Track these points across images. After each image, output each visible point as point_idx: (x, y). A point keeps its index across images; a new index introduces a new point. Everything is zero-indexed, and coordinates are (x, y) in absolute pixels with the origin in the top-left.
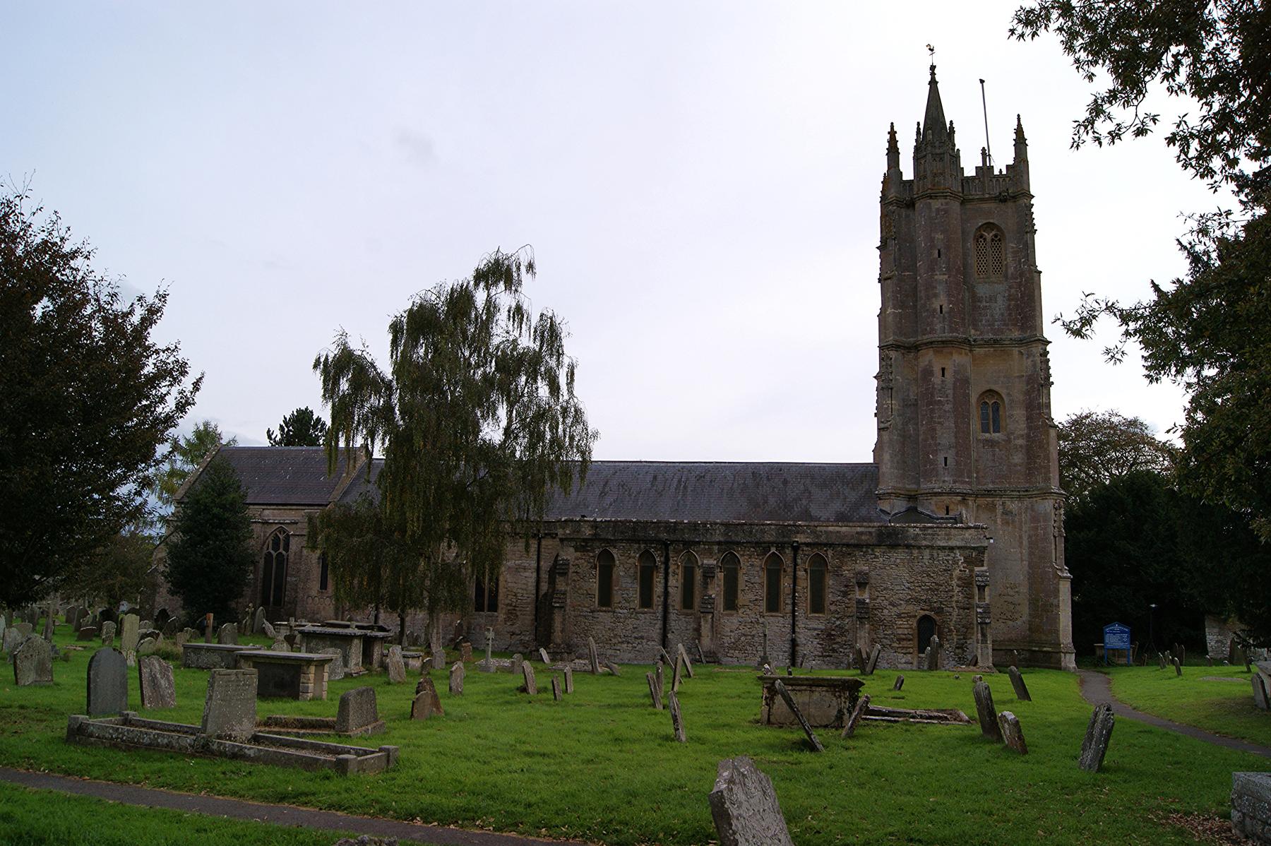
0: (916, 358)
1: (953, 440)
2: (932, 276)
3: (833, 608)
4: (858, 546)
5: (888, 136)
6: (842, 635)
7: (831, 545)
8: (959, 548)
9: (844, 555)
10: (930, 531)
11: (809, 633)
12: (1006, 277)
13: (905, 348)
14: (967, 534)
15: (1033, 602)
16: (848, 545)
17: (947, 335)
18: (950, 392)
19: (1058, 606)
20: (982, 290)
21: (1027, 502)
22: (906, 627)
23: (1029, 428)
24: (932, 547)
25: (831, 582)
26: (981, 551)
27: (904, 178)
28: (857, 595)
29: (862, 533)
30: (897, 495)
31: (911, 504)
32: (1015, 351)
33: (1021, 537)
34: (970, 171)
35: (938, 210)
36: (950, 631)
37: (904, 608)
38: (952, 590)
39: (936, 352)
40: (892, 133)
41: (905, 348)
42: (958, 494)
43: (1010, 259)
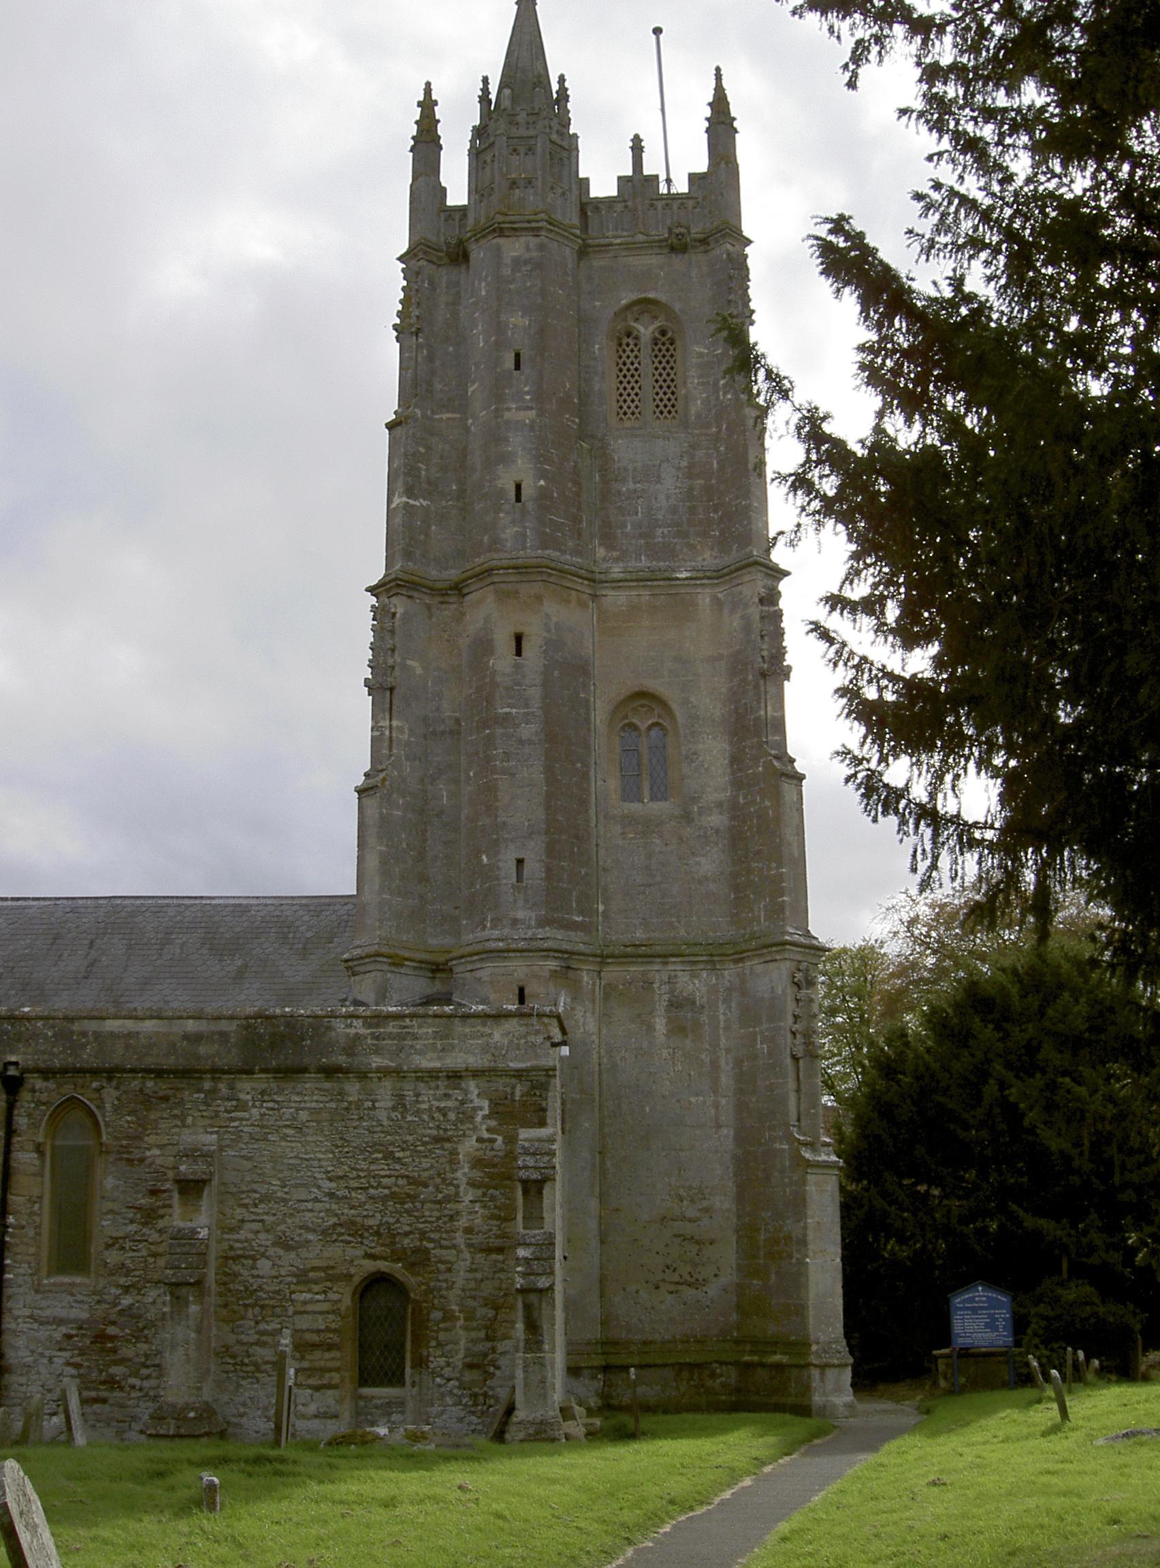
0: (460, 617)
1: (541, 814)
2: (497, 413)
3: (113, 1257)
4: (188, 1074)
5: (417, 113)
6: (138, 1336)
7: (110, 1073)
8: (477, 1074)
9: (148, 1101)
10: (392, 1028)
11: (43, 1333)
12: (685, 424)
13: (433, 591)
14: (498, 1034)
15: (747, 1232)
16: (159, 1073)
17: (531, 553)
18: (535, 693)
19: (803, 1242)
20: (627, 451)
21: (730, 973)
22: (326, 1309)
23: (737, 784)
24: (397, 1073)
25: (110, 1182)
26: (538, 1080)
27: (450, 202)
28: (177, 1218)
29: (197, 1038)
30: (397, 962)
31: (438, 987)
32: (704, 598)
33: (715, 1065)
34: (603, 186)
35: (517, 263)
36: (448, 1317)
37: (317, 1254)
38: (456, 1198)
39: (504, 596)
40: (428, 105)
41: (433, 591)
42: (547, 952)
43: (694, 381)
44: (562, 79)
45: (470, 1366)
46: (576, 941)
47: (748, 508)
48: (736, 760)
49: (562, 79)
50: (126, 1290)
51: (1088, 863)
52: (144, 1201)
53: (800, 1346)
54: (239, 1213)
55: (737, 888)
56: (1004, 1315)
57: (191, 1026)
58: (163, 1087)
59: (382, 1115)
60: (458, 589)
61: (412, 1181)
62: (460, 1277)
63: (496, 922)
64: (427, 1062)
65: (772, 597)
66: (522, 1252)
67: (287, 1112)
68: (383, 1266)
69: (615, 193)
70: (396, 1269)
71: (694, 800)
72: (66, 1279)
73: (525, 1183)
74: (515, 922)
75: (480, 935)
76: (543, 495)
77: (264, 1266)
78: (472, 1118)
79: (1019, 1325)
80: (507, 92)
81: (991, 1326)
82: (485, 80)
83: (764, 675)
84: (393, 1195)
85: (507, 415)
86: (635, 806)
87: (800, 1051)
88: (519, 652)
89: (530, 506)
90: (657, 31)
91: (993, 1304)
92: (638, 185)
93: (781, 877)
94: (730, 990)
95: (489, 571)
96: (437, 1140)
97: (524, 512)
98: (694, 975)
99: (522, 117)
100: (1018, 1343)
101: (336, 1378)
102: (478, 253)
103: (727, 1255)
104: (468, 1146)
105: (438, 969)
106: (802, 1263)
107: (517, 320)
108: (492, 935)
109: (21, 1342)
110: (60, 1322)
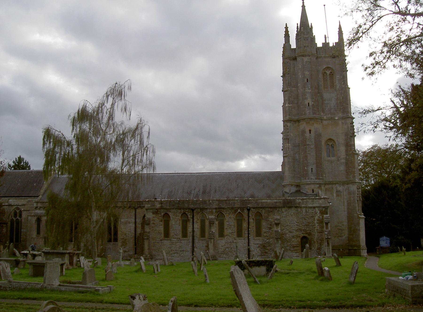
1: (315, 161)
3: (265, 235)
4: (275, 208)
6: (269, 246)
7: (263, 208)
8: (317, 207)
10: (305, 201)
11: (255, 246)
16: (271, 208)
17: (312, 116)
18: (313, 140)
19: (359, 230)
20: (326, 96)
21: (346, 186)
22: (296, 241)
23: (347, 155)
24: (306, 207)
25: (264, 224)
26: (326, 208)
28: (275, 229)
29: (276, 202)
30: (292, 185)
31: (298, 189)
32: (340, 122)
33: (344, 201)
34: (319, 45)
35: (306, 62)
36: (314, 242)
38: (315, 225)
39: (307, 123)
40: (286, 28)
43: (337, 82)
44: (311, 24)
45: (318, 249)
46: (321, 182)
47: (348, 107)
48: (346, 151)
49: (311, 24)
50: (267, 239)
51: (398, 118)
52: (269, 226)
53: (359, 246)
54: (283, 228)
55: (347, 172)
56: (388, 241)
57: (275, 201)
58: (271, 210)
59: (304, 213)
60: (298, 121)
61: (308, 223)
62: (316, 237)
63: (308, 179)
64: (310, 206)
65: (353, 123)
66: (326, 233)
67: (290, 213)
68: (305, 235)
69: (322, 46)
70: (307, 235)
71: (339, 157)
72: (258, 238)
73: (326, 223)
74: (311, 179)
75: (305, 181)
76: (313, 105)
77: (287, 235)
78: (317, 213)
79: (391, 243)
80: (302, 28)
81: (386, 243)
82: (297, 24)
83: (351, 137)
84: (306, 225)
85: (306, 91)
86: (329, 158)
87: (358, 200)
88: (310, 133)
89: (311, 107)
90: (324, 5)
91: (386, 240)
92: (326, 44)
93: (355, 171)
94: (346, 189)
95: (305, 119)
96: (312, 217)
97: (310, 108)
98: (340, 187)
99: (306, 33)
100: (391, 246)
101: (298, 251)
102: (299, 59)
103: (346, 232)
104: (316, 218)
105: (298, 186)
106: (359, 233)
107: (307, 73)
108: (308, 181)
109: (252, 247)
110: (258, 244)
